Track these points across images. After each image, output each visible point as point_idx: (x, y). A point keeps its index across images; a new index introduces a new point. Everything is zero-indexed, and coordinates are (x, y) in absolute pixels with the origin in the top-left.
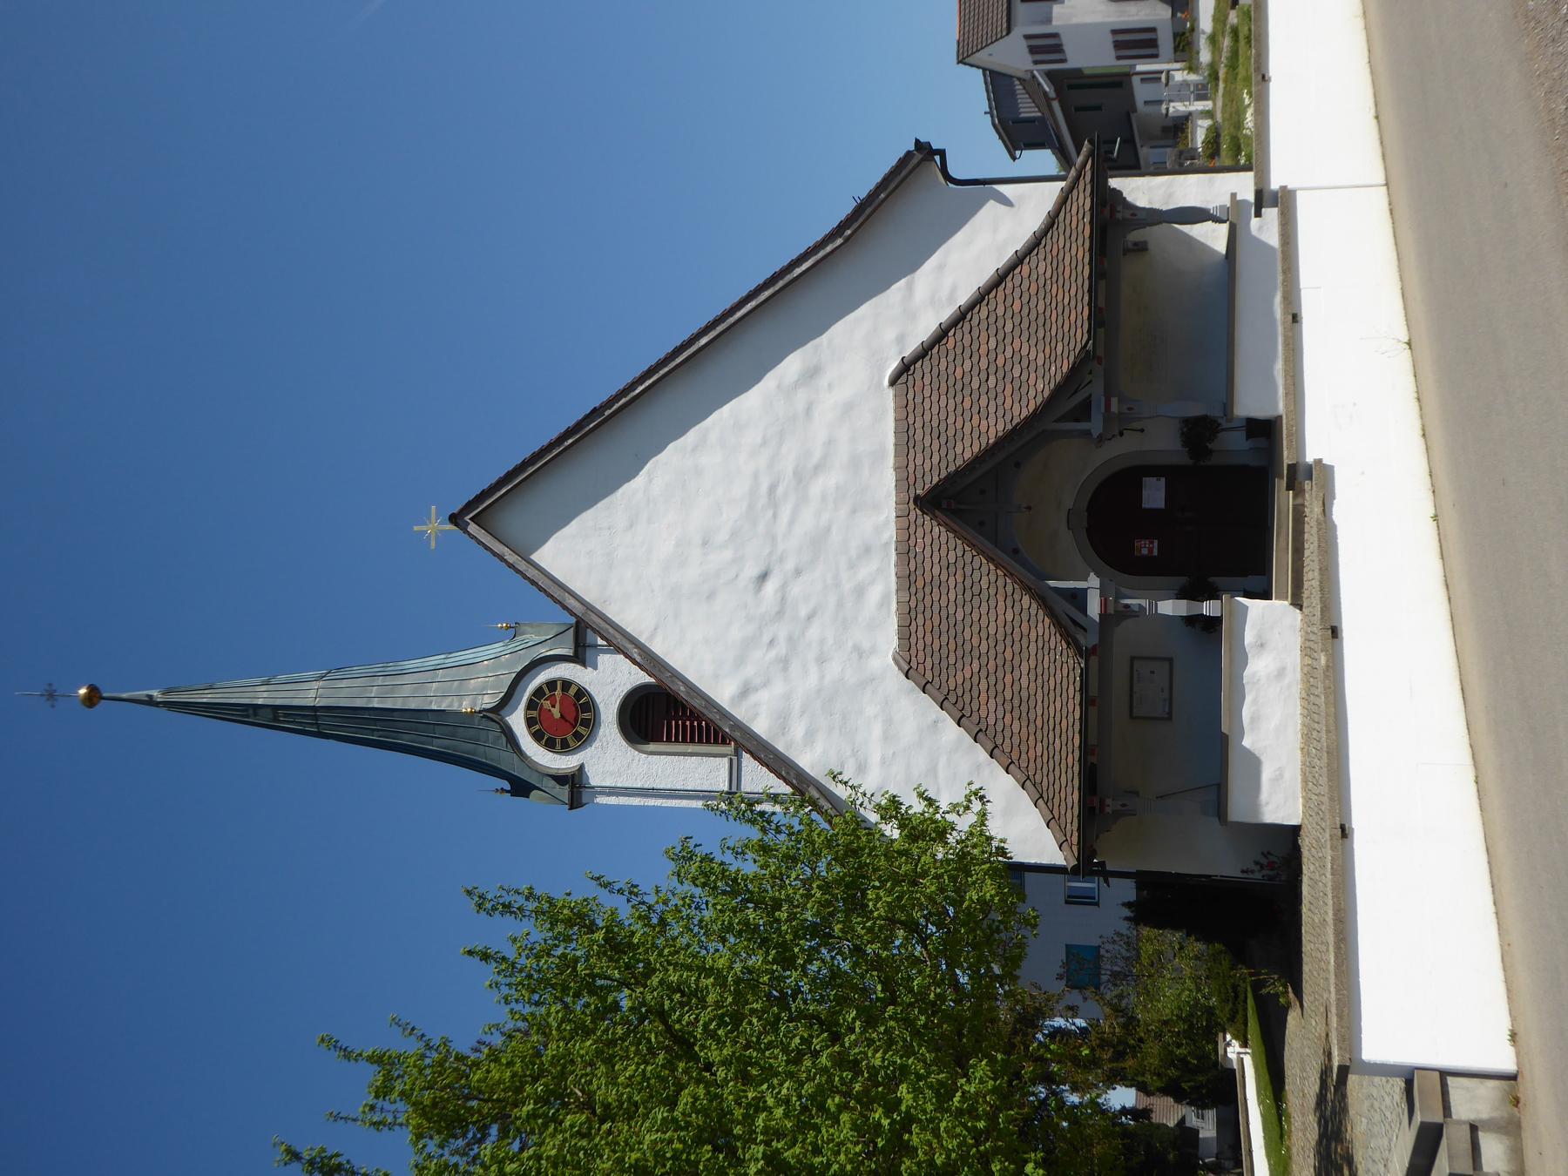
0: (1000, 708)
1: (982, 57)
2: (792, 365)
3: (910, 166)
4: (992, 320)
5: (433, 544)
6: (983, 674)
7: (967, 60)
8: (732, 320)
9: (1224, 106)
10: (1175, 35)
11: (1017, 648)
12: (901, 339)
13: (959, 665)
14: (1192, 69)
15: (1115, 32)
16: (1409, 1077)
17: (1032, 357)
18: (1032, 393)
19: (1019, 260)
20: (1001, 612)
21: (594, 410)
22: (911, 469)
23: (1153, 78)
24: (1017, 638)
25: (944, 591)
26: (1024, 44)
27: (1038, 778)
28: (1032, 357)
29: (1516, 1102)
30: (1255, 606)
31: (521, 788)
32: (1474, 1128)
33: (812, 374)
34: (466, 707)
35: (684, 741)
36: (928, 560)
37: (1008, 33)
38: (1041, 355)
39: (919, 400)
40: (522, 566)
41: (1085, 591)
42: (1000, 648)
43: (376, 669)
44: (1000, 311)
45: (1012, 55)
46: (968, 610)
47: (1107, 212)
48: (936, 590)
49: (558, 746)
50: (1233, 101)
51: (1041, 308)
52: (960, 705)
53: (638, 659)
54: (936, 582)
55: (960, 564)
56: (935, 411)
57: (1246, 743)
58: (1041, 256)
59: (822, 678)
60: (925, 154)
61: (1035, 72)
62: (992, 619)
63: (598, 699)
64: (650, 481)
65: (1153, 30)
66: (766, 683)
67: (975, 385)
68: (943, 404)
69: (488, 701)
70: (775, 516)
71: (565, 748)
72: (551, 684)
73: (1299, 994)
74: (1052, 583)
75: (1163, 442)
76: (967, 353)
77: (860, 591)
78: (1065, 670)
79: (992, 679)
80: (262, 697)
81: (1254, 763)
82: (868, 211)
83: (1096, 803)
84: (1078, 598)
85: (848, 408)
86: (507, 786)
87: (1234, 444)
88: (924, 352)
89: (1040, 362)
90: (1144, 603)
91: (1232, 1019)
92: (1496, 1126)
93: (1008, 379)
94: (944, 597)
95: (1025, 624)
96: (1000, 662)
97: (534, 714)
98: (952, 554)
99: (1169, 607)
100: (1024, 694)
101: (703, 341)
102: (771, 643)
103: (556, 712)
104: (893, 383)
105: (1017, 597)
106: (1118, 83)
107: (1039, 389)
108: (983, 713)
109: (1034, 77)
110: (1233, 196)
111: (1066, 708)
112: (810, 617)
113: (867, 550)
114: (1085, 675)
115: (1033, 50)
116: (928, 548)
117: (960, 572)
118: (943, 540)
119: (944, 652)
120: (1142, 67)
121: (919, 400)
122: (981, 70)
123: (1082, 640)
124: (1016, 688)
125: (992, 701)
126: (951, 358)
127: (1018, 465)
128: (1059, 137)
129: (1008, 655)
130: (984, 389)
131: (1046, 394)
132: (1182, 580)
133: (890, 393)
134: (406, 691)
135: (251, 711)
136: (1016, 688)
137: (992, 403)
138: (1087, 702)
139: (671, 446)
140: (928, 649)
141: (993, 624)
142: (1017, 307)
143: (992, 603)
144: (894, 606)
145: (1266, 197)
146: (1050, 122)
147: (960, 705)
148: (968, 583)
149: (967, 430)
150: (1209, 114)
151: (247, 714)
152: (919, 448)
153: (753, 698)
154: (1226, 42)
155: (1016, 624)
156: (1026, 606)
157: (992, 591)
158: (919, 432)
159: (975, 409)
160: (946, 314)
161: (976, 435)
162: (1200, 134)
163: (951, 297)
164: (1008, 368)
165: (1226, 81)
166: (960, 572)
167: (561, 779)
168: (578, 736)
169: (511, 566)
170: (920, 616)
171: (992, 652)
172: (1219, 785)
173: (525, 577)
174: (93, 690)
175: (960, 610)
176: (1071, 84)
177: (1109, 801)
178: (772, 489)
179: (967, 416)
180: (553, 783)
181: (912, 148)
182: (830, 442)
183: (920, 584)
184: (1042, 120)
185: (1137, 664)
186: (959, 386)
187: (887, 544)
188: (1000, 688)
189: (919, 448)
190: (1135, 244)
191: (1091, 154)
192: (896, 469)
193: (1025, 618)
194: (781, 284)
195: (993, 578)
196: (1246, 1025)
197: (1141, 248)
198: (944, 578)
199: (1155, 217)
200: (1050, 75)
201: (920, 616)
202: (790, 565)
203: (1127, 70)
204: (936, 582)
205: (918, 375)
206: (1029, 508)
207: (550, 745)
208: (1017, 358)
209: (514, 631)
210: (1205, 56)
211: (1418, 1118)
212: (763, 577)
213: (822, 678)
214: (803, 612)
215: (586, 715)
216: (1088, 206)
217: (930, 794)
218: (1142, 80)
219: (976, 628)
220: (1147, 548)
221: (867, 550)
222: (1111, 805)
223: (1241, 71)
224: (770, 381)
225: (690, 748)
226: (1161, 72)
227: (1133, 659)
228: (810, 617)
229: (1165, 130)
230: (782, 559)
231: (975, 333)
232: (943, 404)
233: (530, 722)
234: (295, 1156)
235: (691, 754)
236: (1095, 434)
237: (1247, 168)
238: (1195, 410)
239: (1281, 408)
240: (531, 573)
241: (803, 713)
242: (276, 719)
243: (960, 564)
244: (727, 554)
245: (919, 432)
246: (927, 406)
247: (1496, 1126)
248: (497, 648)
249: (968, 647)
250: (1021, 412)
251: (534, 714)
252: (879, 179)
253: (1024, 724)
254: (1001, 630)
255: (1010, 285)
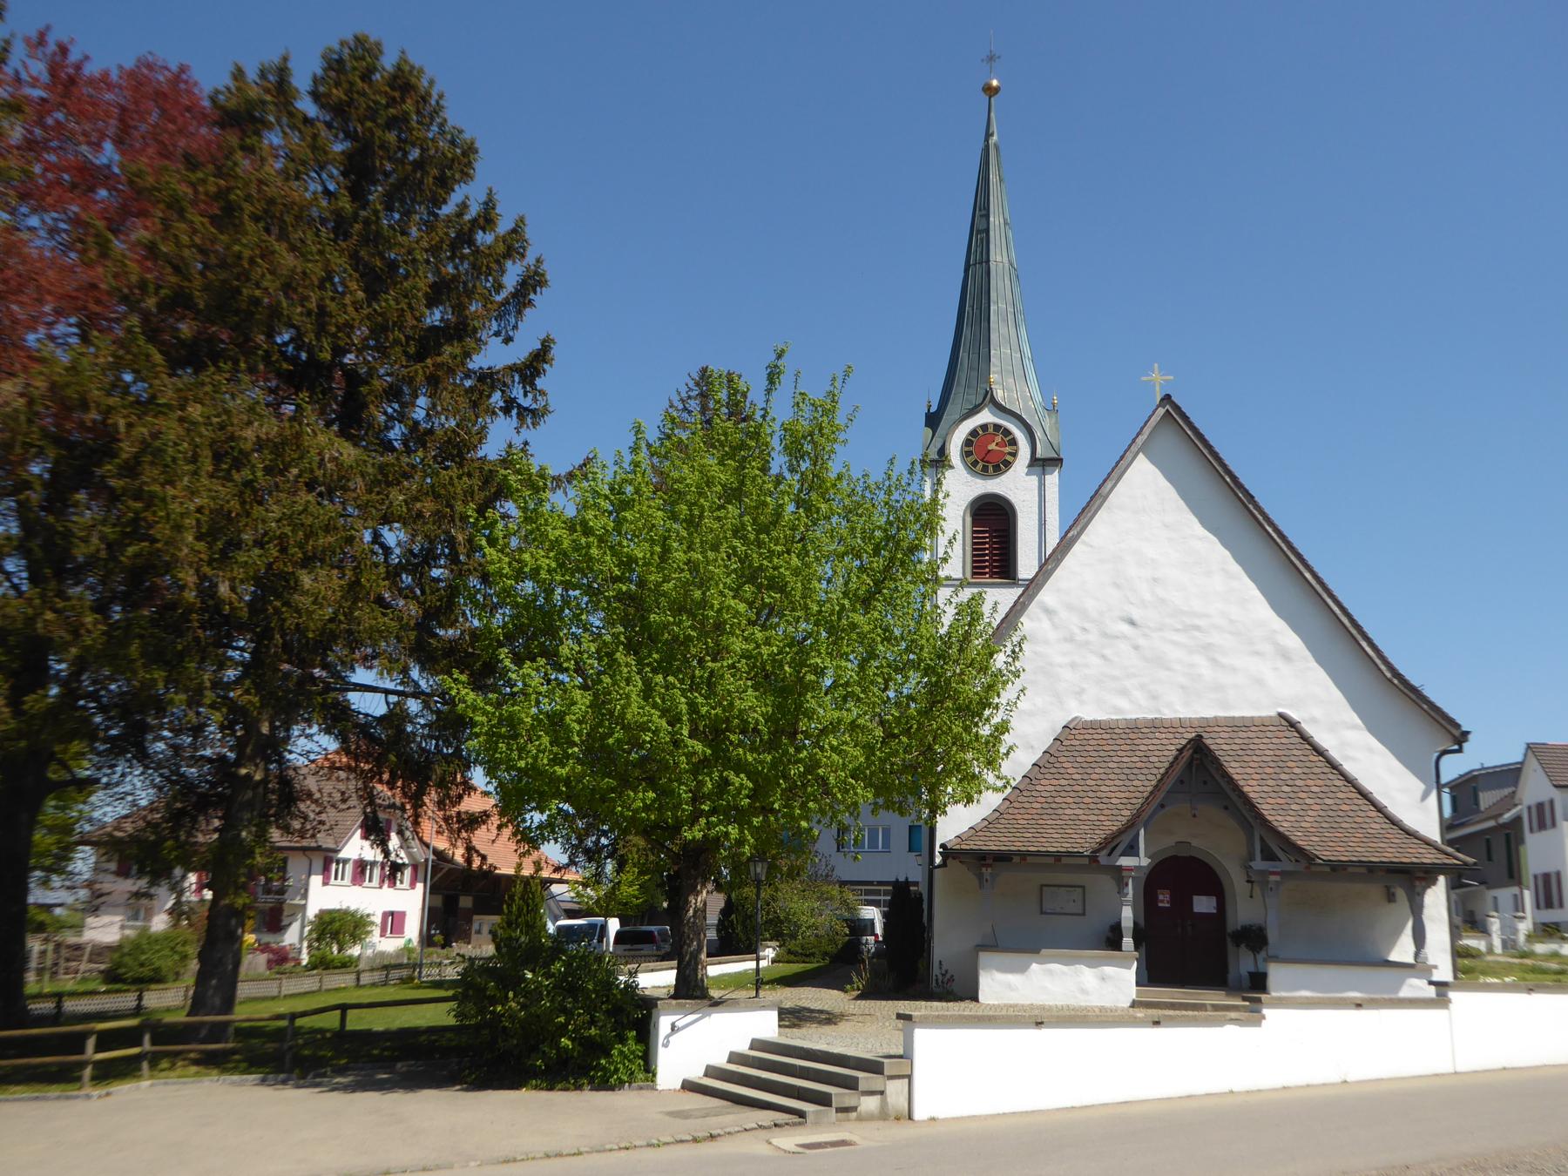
0: (1048, 794)
1: (1533, 764)
2: (1292, 641)
3: (1449, 727)
4: (1333, 789)
5: (1145, 379)
6: (1071, 782)
7: (1530, 752)
8: (1325, 596)
9: (1499, 963)
10: (1557, 924)
11: (1092, 806)
12: (1314, 720)
13: (1076, 765)
14: (1530, 938)
15: (1558, 874)
16: (907, 1056)
17: (1307, 819)
18: (1280, 818)
19: (1380, 809)
20: (1118, 794)
21: (1252, 497)
22: (1216, 729)
23: (1518, 905)
24: (1099, 806)
25: (1128, 754)
26: (1544, 798)
27: (1003, 821)
28: (1307, 819)
29: (897, 1119)
30: (1129, 975)
31: (933, 420)
32: (882, 1093)
33: (1286, 656)
34: (993, 377)
35: (974, 544)
36: (1150, 742)
37: (1556, 786)
38: (1308, 825)
39: (1269, 734)
40: (1134, 449)
41: (1137, 855)
42: (1091, 794)
43: (1019, 306)
44: (1340, 795)
45: (1535, 788)
46: (1116, 771)
47: (1421, 875)
48: (1128, 748)
49: (967, 449)
50: (1507, 969)
51: (1344, 825)
52: (1047, 765)
53: (1070, 535)
54: (1134, 748)
55: (1148, 765)
56: (1261, 747)
57: (1034, 966)
58: (1384, 826)
59: (1060, 666)
60: (1460, 738)
61: (1519, 807)
62: (1112, 789)
63: (1003, 477)
64: (1200, 539)
65: (1561, 905)
66: (1055, 627)
67: (1283, 776)
68: (1267, 752)
69: (999, 395)
70: (1177, 630)
71: (966, 454)
72: (1013, 442)
73: (858, 998)
74: (1142, 832)
75: (1243, 912)
76: (1306, 770)
77: (1124, 692)
78: (1083, 840)
79: (1068, 788)
80: (995, 220)
81: (1022, 969)
82: (1413, 697)
83: (989, 861)
84: (1132, 850)
85: (1259, 682)
86: (933, 410)
87: (1243, 963)
88: (1305, 738)
89: (1303, 824)
90: (1130, 897)
91: (790, 952)
92: (884, 1104)
93: (1289, 801)
94: (1124, 754)
95: (1109, 812)
96: (1081, 794)
97: (991, 430)
98: (1156, 759)
99: (1127, 915)
100: (1060, 812)
101: (1308, 575)
102: (1084, 629)
103: (992, 446)
104: (1281, 715)
105: (1129, 806)
106: (1513, 875)
107: (1284, 824)
108: (1043, 782)
109: (1516, 805)
110: (1435, 967)
111: (1054, 843)
112: (1104, 657)
113: (1154, 697)
114: (1079, 855)
115: (1540, 806)
116: (1158, 742)
117: (1143, 765)
118: (1166, 753)
119: (1085, 754)
120: (1528, 896)
121: (1269, 734)
122: (1520, 759)
123: (1105, 852)
124: (1064, 806)
125: (1052, 788)
126: (1302, 758)
127: (1226, 808)
128: (1462, 825)
129: (1086, 800)
130: (1280, 783)
131: (1281, 829)
132: (1142, 922)
133: (1273, 713)
134: (1003, 330)
135: (983, 212)
136: (1064, 806)
137: (1270, 789)
138: (1058, 856)
139: (1227, 553)
140: (1085, 742)
141: (1107, 789)
142: (1344, 807)
143: (1123, 789)
144: (1114, 717)
145: (1442, 989)
146: (1476, 817)
147: (1047, 765)
148: (1135, 771)
149: (1249, 770)
150: (1490, 950)
151: (981, 208)
152: (1232, 735)
153: (1043, 616)
154: (1554, 966)
155: (1110, 806)
156: (1123, 813)
157: (1132, 789)
158: (1245, 735)
159: (1264, 776)
160: (1334, 754)
161: (1245, 777)
162: (1473, 942)
163: (1347, 758)
164: (1297, 801)
165: (1521, 964)
166: (1143, 765)
167: (942, 451)
168: (975, 464)
169: (1134, 441)
170: (1108, 736)
171: (1087, 788)
172: (997, 946)
173: (1126, 451)
174: (997, 90)
175: (1115, 765)
176: (1511, 835)
177: (989, 870)
178: (1197, 628)
179: (1260, 771)
180: (939, 446)
181: (1464, 729)
182: (1234, 670)
183: (1132, 736)
184: (1478, 811)
185: (1080, 890)
186: (1281, 764)
187: (1159, 711)
188: (1063, 794)
189: (1232, 735)
190: (1393, 895)
191: (1465, 864)
192: (1215, 718)
193: (1114, 812)
194: (1354, 632)
195: (1141, 789)
196: (788, 962)
197: (1391, 898)
198: (1138, 753)
199: (1417, 910)
200: (1518, 820)
201: (1108, 736)
202: (1141, 642)
203: (1524, 880)
204: (1134, 748)
205: (1287, 734)
206: (1194, 816)
207: (968, 443)
208: (1305, 807)
209: (1052, 410)
210: (1540, 948)
211: (885, 1061)
212: (1132, 623)
213: (1060, 666)
214: (1107, 652)
215: (991, 469)
216: (1425, 861)
217: (1012, 754)
218: (1515, 896)
219: (1103, 777)
220: (1164, 899)
221: (1154, 697)
222: (987, 872)
223: (1530, 976)
224: (1278, 624)
225: (969, 549)
226: (1523, 911)
227: (1083, 887)
228: (1104, 657)
229: (1472, 913)
230: (1145, 635)
231: (1322, 776)
232: (1267, 752)
233: (984, 427)
234: (779, 356)
235: (964, 550)
236: (1252, 864)
237: (1455, 977)
238: (1272, 935)
239: (1274, 994)
240: (1129, 455)
241: (1035, 653)
242: (979, 232)
243: (1148, 765)
244: (1148, 596)
245: (1245, 735)
246: (1265, 741)
247: (884, 1104)
248: (1038, 397)
249: (1089, 771)
250: (1266, 809)
251: (991, 430)
252: (1439, 704)
253: (1039, 811)
254: (1104, 795)
255: (1360, 802)
